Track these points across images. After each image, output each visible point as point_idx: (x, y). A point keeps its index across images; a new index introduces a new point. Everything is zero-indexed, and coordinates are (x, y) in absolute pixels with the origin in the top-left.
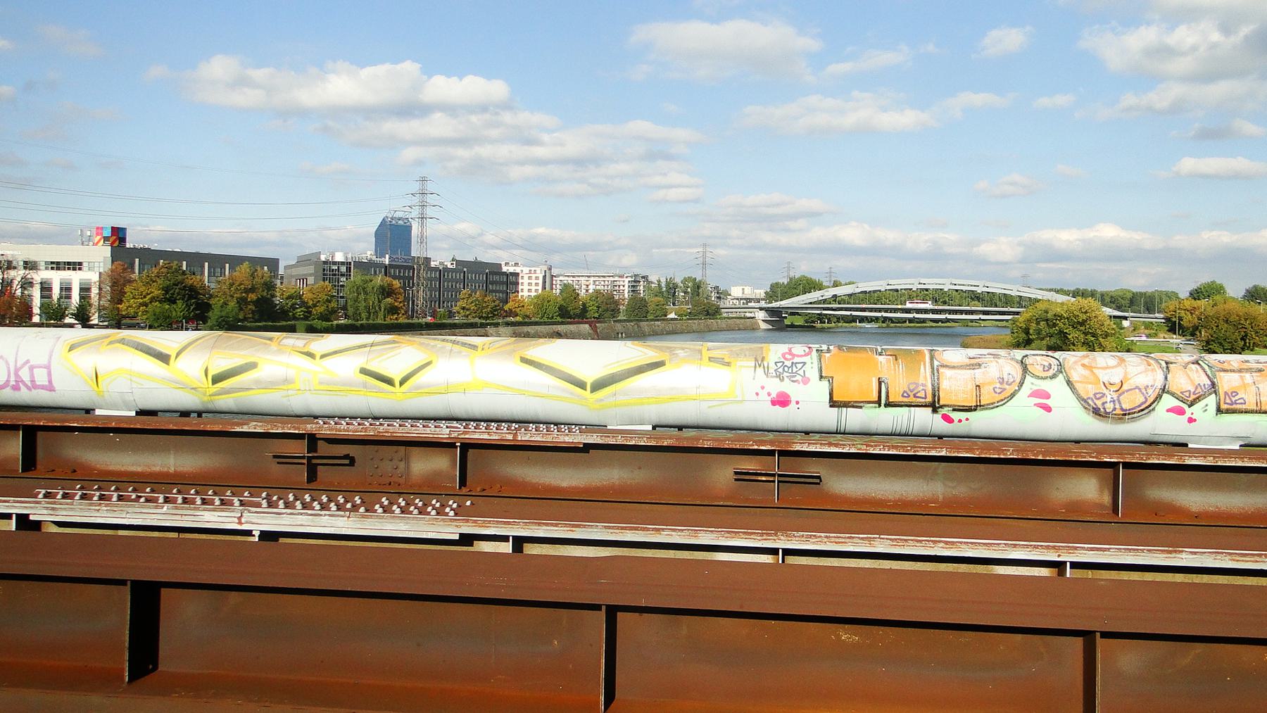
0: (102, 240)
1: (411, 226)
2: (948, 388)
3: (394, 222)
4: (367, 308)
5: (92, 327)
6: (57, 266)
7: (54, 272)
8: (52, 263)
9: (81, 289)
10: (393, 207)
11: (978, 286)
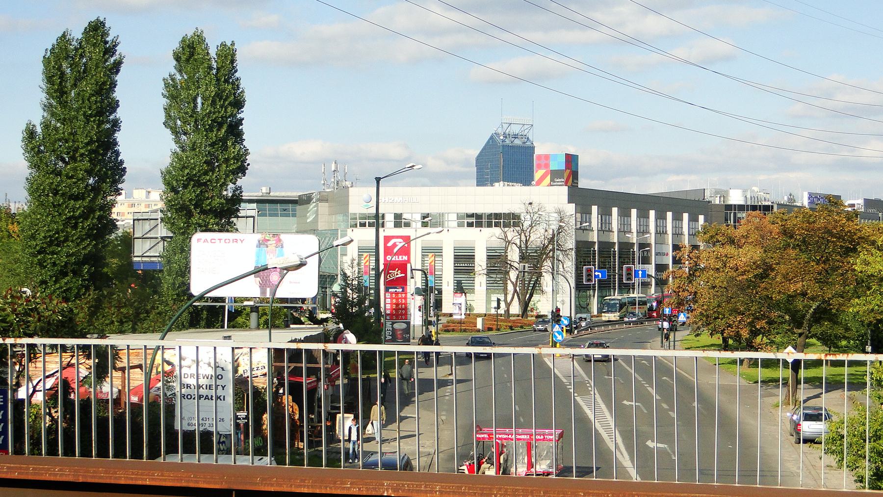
0: (549, 178)
1: (533, 148)
2: (120, 380)
3: (508, 142)
4: (729, 319)
5: (868, 353)
6: (477, 220)
7: (474, 230)
8: (472, 216)
9: (457, 258)
10: (507, 118)
11: (481, 283)
